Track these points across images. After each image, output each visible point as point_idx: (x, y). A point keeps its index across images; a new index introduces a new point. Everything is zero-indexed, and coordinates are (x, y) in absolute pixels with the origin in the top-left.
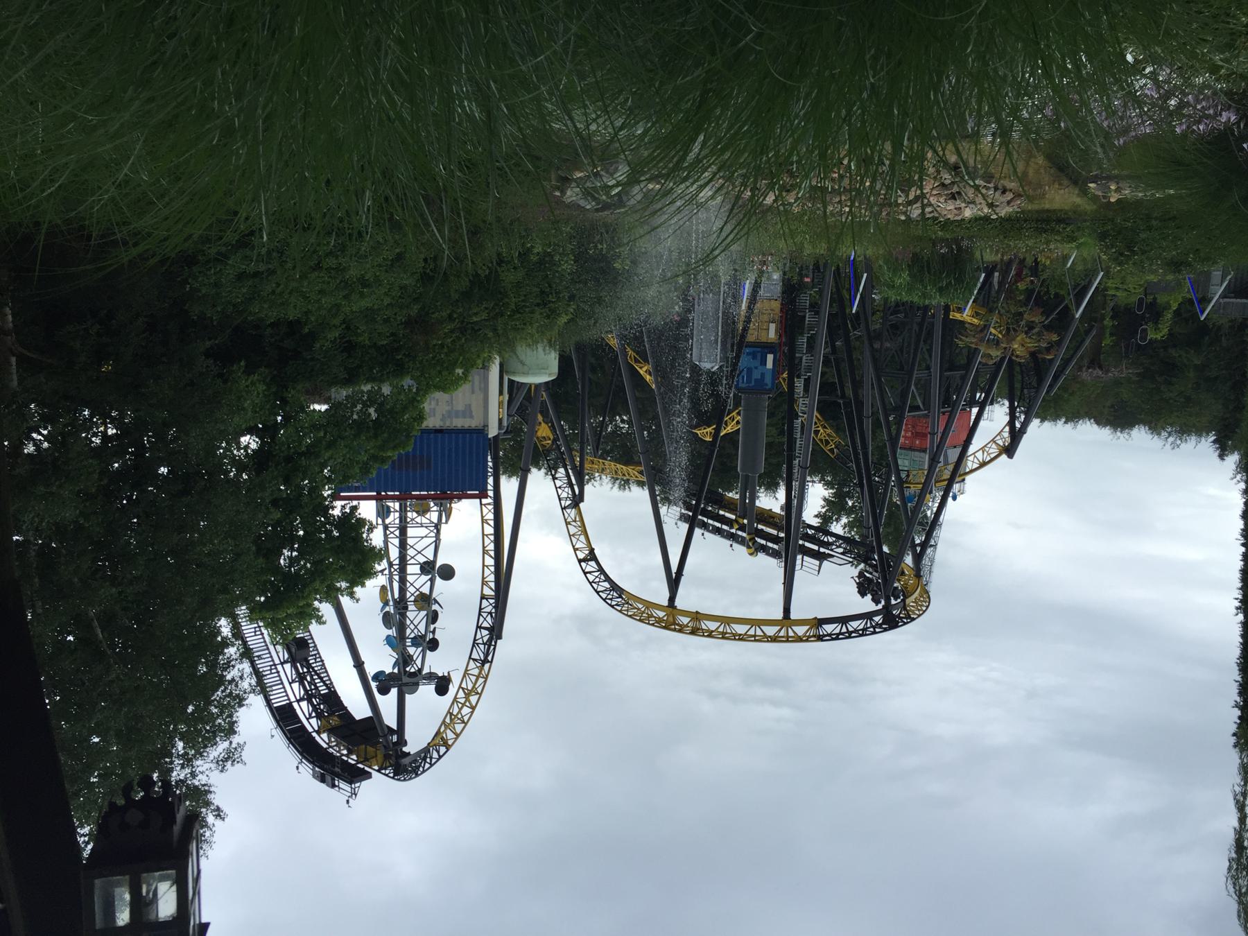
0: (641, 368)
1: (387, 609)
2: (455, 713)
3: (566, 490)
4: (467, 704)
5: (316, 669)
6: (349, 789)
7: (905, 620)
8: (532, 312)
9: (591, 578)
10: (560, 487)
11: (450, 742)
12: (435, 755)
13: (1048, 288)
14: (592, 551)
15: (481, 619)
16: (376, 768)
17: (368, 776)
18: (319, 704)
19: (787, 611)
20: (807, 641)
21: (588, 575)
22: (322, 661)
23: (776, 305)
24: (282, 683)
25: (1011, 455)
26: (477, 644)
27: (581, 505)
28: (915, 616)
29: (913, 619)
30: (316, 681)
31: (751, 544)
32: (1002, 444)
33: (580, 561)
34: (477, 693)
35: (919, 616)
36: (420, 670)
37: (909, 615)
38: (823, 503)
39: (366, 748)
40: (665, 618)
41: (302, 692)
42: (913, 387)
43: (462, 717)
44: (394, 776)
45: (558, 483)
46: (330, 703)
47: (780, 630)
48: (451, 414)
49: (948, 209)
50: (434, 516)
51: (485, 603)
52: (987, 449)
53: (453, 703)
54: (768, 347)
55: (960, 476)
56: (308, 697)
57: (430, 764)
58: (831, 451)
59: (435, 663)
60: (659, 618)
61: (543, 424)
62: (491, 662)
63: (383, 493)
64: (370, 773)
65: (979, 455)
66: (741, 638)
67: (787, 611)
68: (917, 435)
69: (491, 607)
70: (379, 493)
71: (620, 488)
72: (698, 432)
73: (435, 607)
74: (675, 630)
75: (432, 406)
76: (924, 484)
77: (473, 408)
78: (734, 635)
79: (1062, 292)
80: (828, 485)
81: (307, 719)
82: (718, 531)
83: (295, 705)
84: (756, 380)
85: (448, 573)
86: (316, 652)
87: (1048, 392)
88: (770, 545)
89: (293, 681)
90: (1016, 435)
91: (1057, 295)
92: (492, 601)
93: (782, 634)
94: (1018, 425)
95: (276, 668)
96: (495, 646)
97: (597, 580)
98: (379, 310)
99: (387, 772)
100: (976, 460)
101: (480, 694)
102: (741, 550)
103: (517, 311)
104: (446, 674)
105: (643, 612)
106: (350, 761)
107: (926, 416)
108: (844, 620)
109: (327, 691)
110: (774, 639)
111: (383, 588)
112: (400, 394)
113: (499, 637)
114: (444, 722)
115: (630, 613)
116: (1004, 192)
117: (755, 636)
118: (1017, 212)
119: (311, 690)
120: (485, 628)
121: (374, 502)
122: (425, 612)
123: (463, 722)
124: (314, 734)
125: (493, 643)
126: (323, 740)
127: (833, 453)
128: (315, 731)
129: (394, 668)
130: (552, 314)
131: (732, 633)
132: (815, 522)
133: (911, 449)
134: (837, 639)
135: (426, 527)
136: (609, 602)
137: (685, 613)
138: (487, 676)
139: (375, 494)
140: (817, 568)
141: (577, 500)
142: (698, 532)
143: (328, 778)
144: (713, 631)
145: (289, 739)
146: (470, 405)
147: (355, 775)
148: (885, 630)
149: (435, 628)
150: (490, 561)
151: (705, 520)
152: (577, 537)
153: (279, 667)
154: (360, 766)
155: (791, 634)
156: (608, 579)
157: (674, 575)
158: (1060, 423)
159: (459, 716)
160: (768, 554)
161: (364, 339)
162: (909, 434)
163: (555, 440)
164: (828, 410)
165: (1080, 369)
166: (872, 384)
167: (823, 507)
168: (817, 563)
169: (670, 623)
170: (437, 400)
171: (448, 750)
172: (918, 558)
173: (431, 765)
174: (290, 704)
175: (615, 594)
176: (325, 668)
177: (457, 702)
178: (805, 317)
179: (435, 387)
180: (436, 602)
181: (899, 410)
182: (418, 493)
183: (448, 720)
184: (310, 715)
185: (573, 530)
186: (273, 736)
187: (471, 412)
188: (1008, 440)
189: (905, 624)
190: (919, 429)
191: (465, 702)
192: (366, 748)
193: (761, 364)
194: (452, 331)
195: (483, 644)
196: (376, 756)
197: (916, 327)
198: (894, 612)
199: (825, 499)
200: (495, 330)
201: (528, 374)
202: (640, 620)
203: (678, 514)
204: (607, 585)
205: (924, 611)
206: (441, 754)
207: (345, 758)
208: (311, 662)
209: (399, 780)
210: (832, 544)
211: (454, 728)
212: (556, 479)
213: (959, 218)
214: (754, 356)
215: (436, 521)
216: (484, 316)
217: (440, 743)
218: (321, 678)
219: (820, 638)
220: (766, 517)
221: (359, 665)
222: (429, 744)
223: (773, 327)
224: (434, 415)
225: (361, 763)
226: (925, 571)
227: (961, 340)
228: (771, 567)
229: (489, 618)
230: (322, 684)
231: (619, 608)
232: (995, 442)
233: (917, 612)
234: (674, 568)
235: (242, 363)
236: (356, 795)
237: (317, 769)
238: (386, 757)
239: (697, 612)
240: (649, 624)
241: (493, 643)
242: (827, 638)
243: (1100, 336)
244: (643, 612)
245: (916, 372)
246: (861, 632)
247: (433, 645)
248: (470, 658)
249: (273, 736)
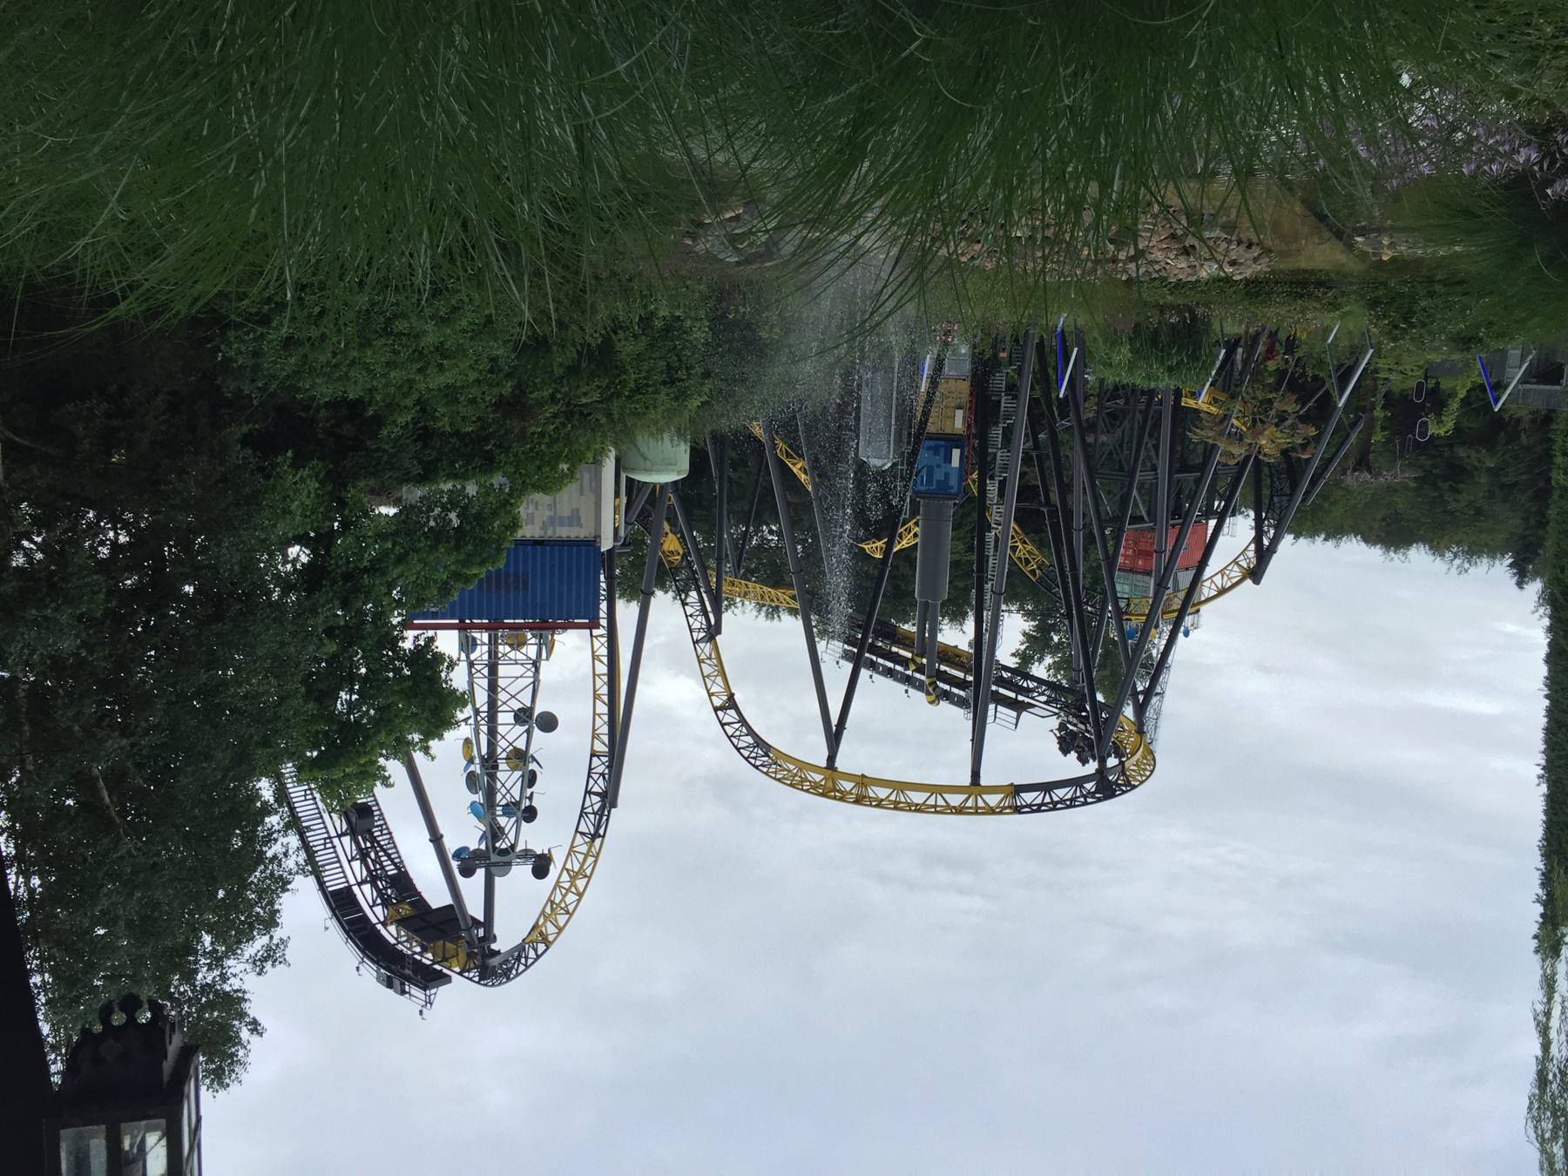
0: (794, 464)
1: (472, 768)
2: (557, 901)
3: (699, 618)
4: (573, 889)
5: (382, 843)
6: (423, 997)
7: (1124, 788)
8: (657, 392)
9: (730, 730)
10: (691, 616)
11: (551, 938)
12: (532, 954)
13: (1304, 369)
14: (731, 696)
15: (591, 782)
16: (457, 969)
17: (446, 979)
18: (385, 888)
19: (976, 774)
20: (1001, 813)
21: (726, 727)
22: (390, 833)
23: (965, 387)
24: (339, 861)
25: (1257, 581)
26: (586, 814)
27: (718, 638)
28: (1137, 783)
29: (1134, 787)
30: (383, 859)
31: (931, 690)
32: (1246, 566)
33: (716, 709)
34: (585, 876)
35: (1142, 782)
36: (513, 847)
37: (1129, 782)
38: (1022, 638)
39: (444, 945)
40: (823, 783)
41: (365, 873)
42: (1135, 493)
43: (567, 906)
44: (480, 980)
45: (689, 610)
46: (400, 886)
47: (967, 800)
48: (552, 521)
49: (1179, 267)
50: (531, 651)
51: (596, 761)
52: (1227, 572)
53: (554, 889)
54: (952, 440)
55: (1194, 605)
56: (373, 879)
57: (525, 965)
58: (1033, 572)
59: (532, 837)
60: (815, 782)
61: (670, 535)
62: (603, 837)
63: (468, 621)
64: (449, 977)
65: (1218, 579)
66: (918, 809)
67: (976, 774)
68: (1141, 553)
69: (603, 767)
70: (462, 621)
71: (767, 616)
72: (866, 547)
73: (533, 766)
74: (835, 798)
75: (530, 511)
76: (1148, 616)
77: (582, 513)
78: (909, 805)
79: (1321, 374)
80: (1029, 615)
81: (371, 907)
82: (889, 673)
83: (356, 889)
84: (938, 481)
85: (549, 723)
86: (382, 822)
87: (1303, 500)
88: (955, 690)
89: (353, 859)
90: (1264, 555)
91: (1315, 378)
92: (605, 759)
93: (969, 804)
94: (1266, 542)
95: (332, 842)
96: (608, 816)
97: (738, 733)
98: (463, 387)
99: (471, 975)
100: (1213, 587)
101: (590, 877)
102: (918, 697)
103: (638, 390)
104: (546, 852)
105: (796, 775)
106: (424, 961)
107: (1152, 529)
108: (1047, 787)
109: (395, 872)
110: (959, 811)
111: (467, 741)
112: (487, 494)
113: (614, 805)
114: (543, 912)
115: (778, 776)
116: (1249, 246)
117: (935, 806)
118: (1266, 273)
119: (376, 870)
120: (596, 794)
121: (456, 632)
122: (521, 773)
123: (567, 912)
124: (379, 927)
125: (606, 813)
126: (390, 933)
127: (1035, 575)
128: (380, 922)
129: (480, 843)
130: (682, 396)
131: (907, 802)
132: (1012, 662)
133: (1132, 571)
134: (1038, 810)
135: (522, 664)
136: (753, 761)
137: (848, 777)
138: (598, 854)
139: (457, 621)
140: (1014, 721)
141: (713, 632)
142: (864, 673)
143: (397, 982)
144: (882, 800)
145: (347, 932)
146: (578, 510)
147: (430, 979)
148: (1099, 800)
149: (532, 793)
150: (603, 709)
151: (874, 658)
152: (713, 678)
153: (336, 841)
154: (437, 967)
155: (981, 804)
156: (751, 732)
157: (834, 728)
158: (1319, 540)
159: (563, 905)
160: (952, 703)
161: (444, 425)
162: (1130, 552)
163: (685, 556)
164: (1029, 520)
165: (1344, 472)
166: (1084, 489)
167: (1022, 644)
168: (1014, 714)
169: (828, 790)
170: (537, 503)
171: (548, 948)
172: (1140, 710)
173: (527, 967)
174: (349, 888)
175: (760, 752)
176: (393, 843)
177: (560, 887)
178: (999, 402)
179: (532, 486)
180: (534, 759)
181: (1118, 521)
182: (512, 621)
183: (548, 910)
184: (374, 901)
185: (707, 670)
186: (327, 928)
187: (579, 518)
188: (1254, 561)
189: (1124, 792)
190: (1142, 546)
191: (570, 887)
192: (444, 945)
193: (945, 462)
194: (555, 416)
195: (594, 813)
196: (457, 955)
197: (1139, 416)
198: (1110, 778)
199: (1025, 634)
200: (609, 415)
201: (651, 470)
202: (791, 785)
203: (840, 650)
204: (750, 740)
205: (1148, 777)
206: (539, 953)
207: (418, 957)
208: (376, 834)
209: (486, 985)
210: (1032, 690)
211: (556, 921)
212: (687, 604)
213: (1193, 279)
214: (936, 450)
215: (534, 657)
216: (596, 396)
217: (538, 940)
218: (389, 856)
219: (1017, 810)
220: (950, 655)
221: (436, 839)
222: (524, 940)
223: (959, 414)
224: (533, 523)
225: (438, 963)
226: (1149, 726)
227: (1195, 433)
228: (957, 719)
229: (601, 781)
230: (385, 858)
231: (765, 770)
232: (1237, 563)
233: (1139, 778)
234: (834, 720)
235: (290, 454)
236: (431, 1004)
237: (382, 970)
238: (470, 956)
239: (863, 776)
240: (802, 790)
241: (606, 813)
242: (1026, 810)
243: (1369, 430)
244: (796, 775)
245: (1138, 473)
246: (1068, 803)
247: (530, 814)
248: (577, 831)
249: (327, 928)
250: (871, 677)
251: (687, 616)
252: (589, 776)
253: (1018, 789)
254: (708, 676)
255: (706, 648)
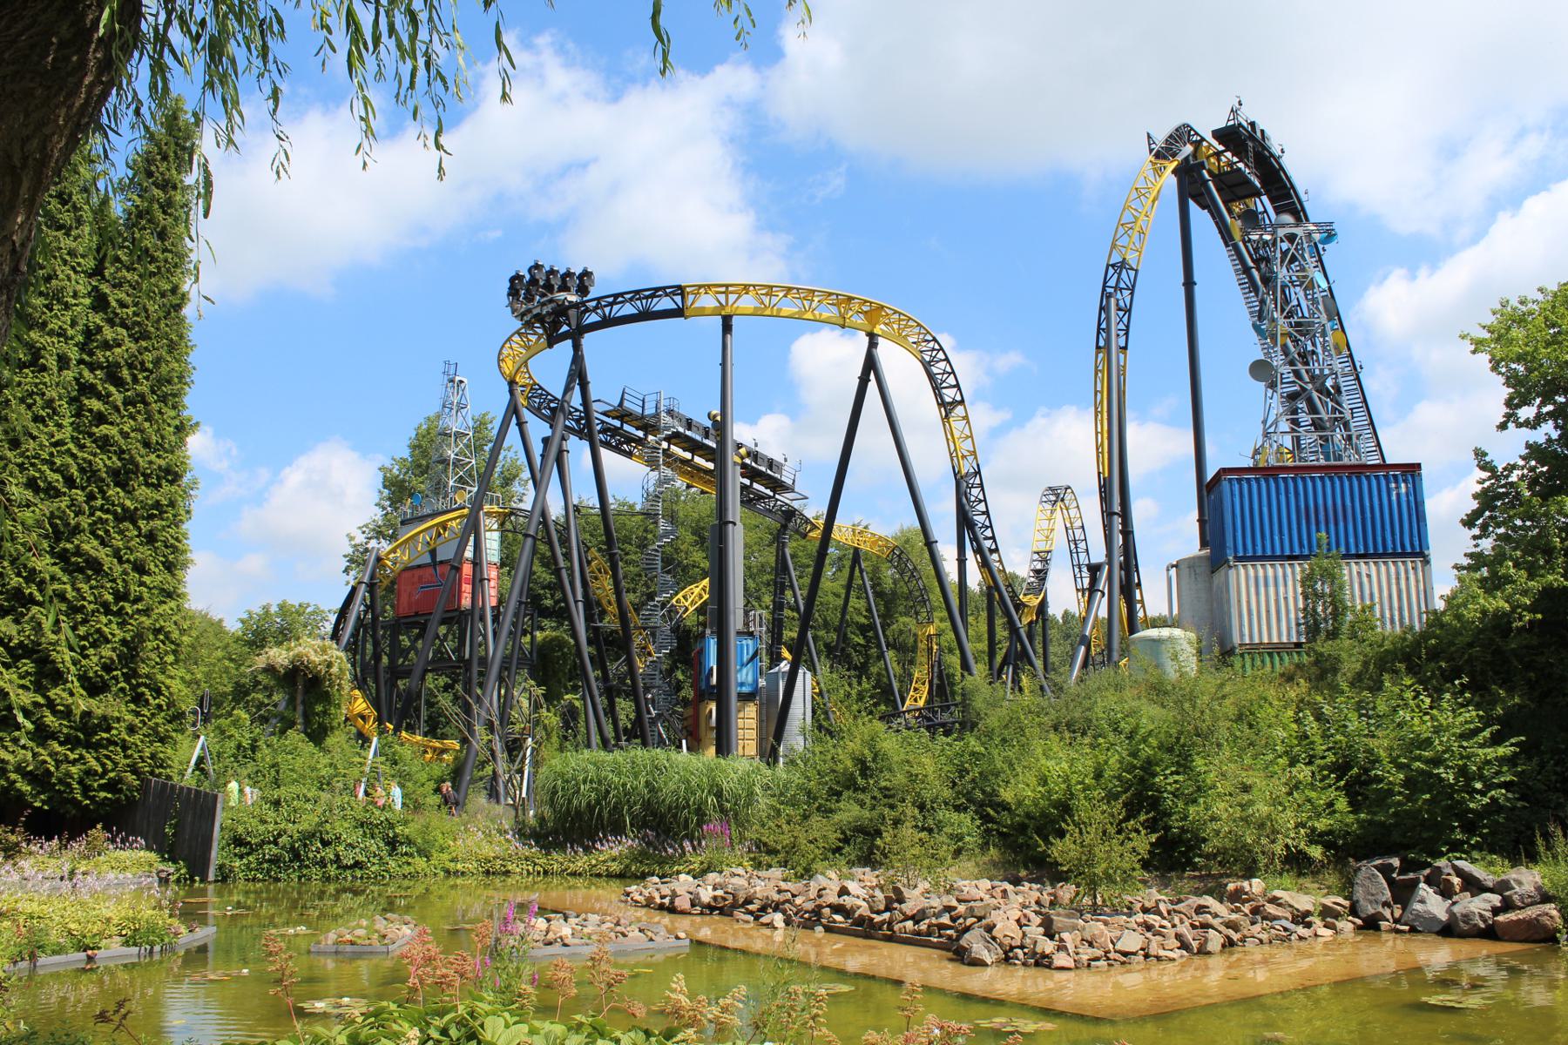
16: (1205, 144)
17: (1217, 134)
33: (962, 402)
108: (645, 315)
134: (616, 296)
136: (937, 347)
140: (626, 396)
155: (678, 299)
212: (983, 513)
219: (680, 290)
234: (872, 376)
250: (756, 445)
251: (985, 500)
252: (1128, 327)
253: (678, 313)
254: (967, 437)
255: (966, 467)
